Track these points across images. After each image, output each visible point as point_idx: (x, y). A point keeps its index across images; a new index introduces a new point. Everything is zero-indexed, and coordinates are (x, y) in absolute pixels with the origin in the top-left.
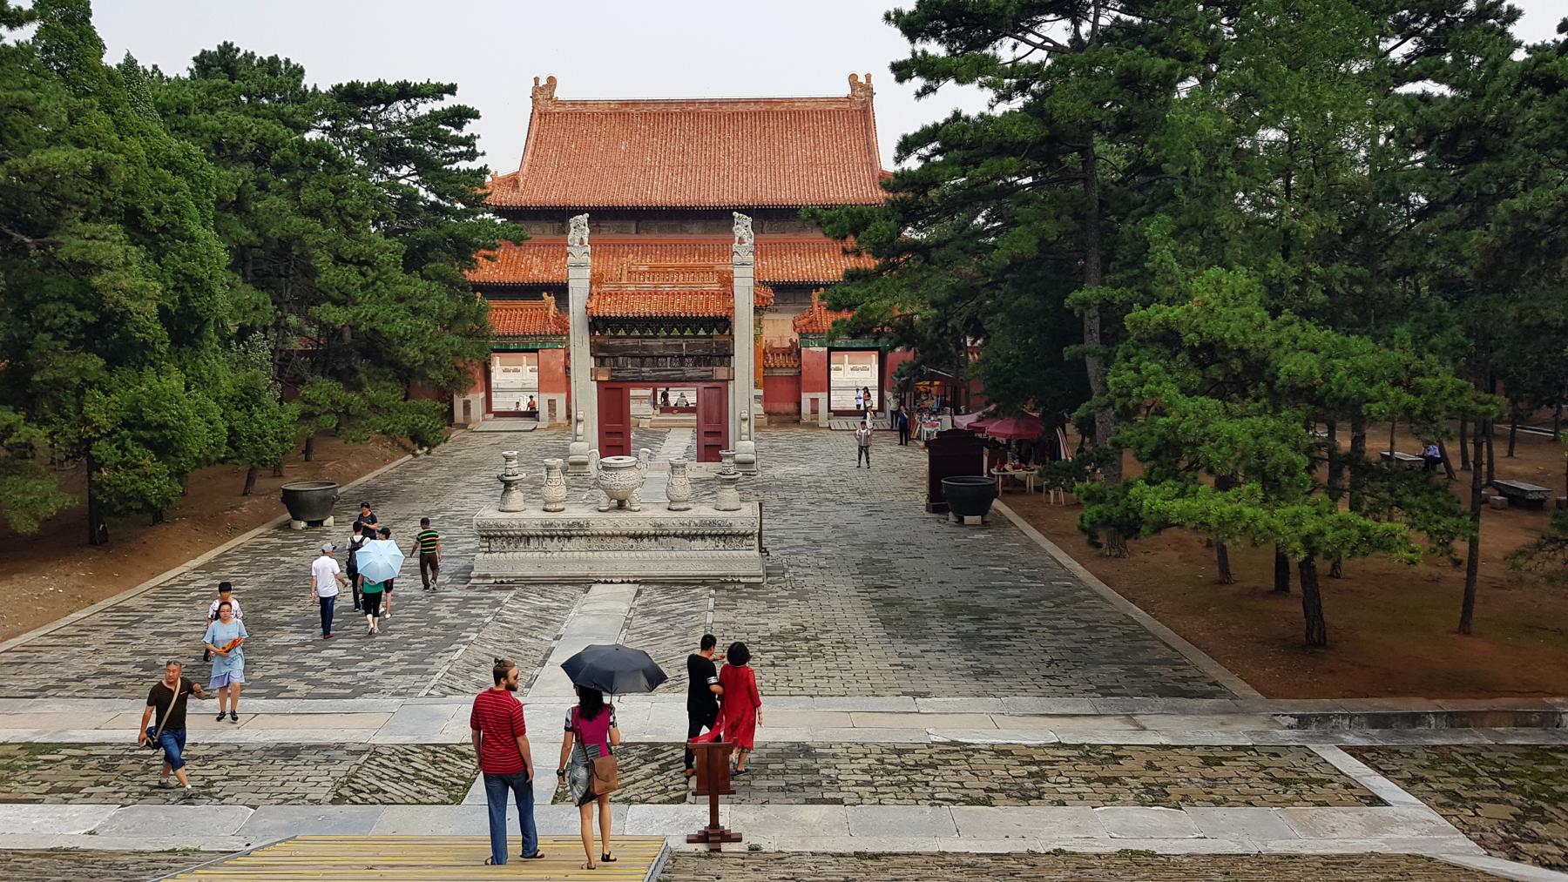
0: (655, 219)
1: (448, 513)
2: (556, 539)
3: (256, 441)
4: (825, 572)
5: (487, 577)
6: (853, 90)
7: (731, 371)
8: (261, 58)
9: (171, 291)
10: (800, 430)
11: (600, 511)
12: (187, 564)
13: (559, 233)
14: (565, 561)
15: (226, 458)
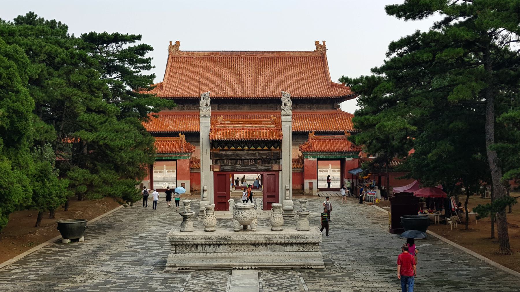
0: (227, 103)
1: (143, 235)
2: (212, 246)
3: (46, 197)
4: (355, 263)
5: (174, 266)
6: (317, 48)
7: (281, 166)
8: (47, 20)
9: (6, 118)
10: (304, 197)
11: (235, 231)
12: (9, 261)
13: (181, 110)
14: (217, 258)
15: (30, 205)
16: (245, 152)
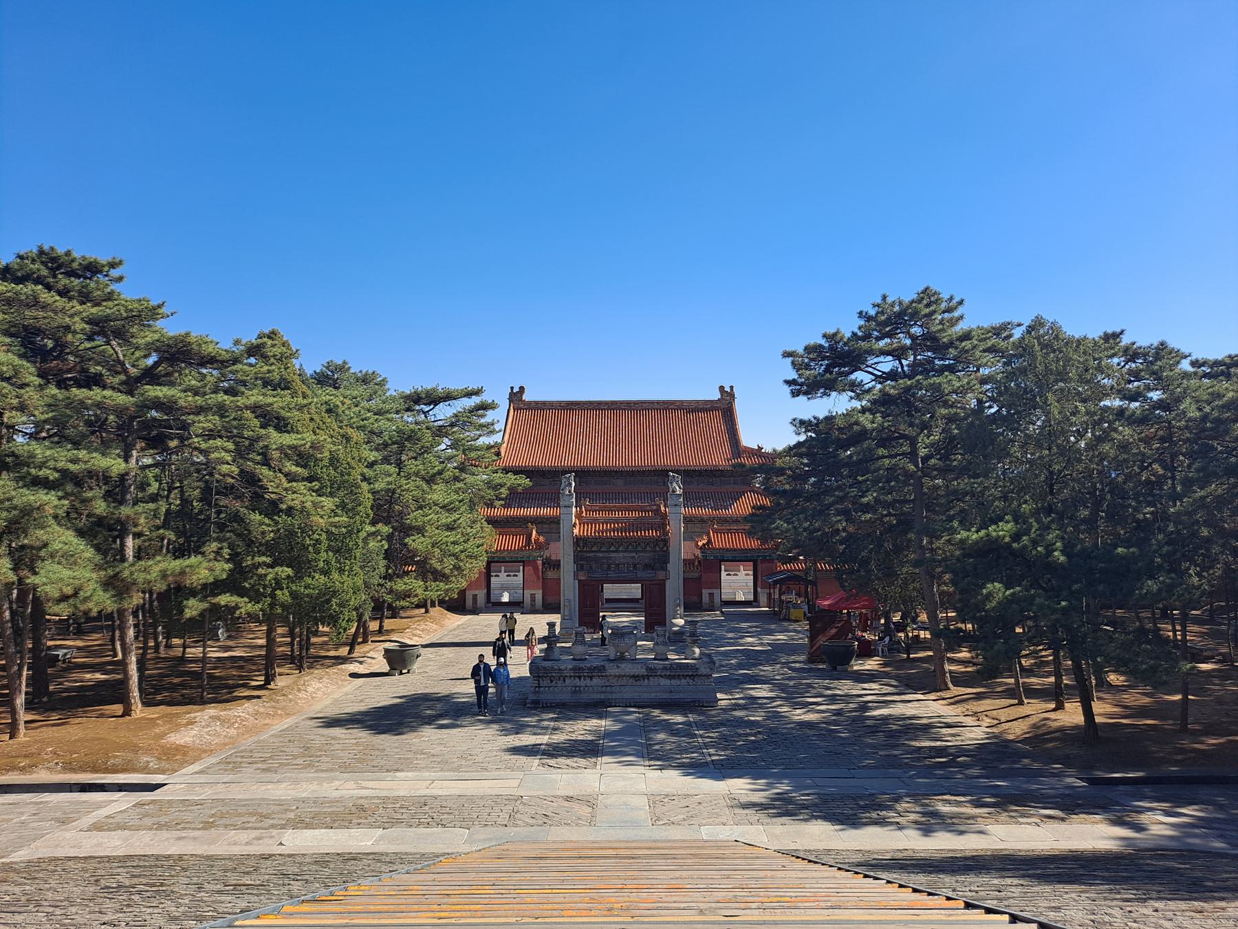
6: (722, 395)
16: (621, 555)
